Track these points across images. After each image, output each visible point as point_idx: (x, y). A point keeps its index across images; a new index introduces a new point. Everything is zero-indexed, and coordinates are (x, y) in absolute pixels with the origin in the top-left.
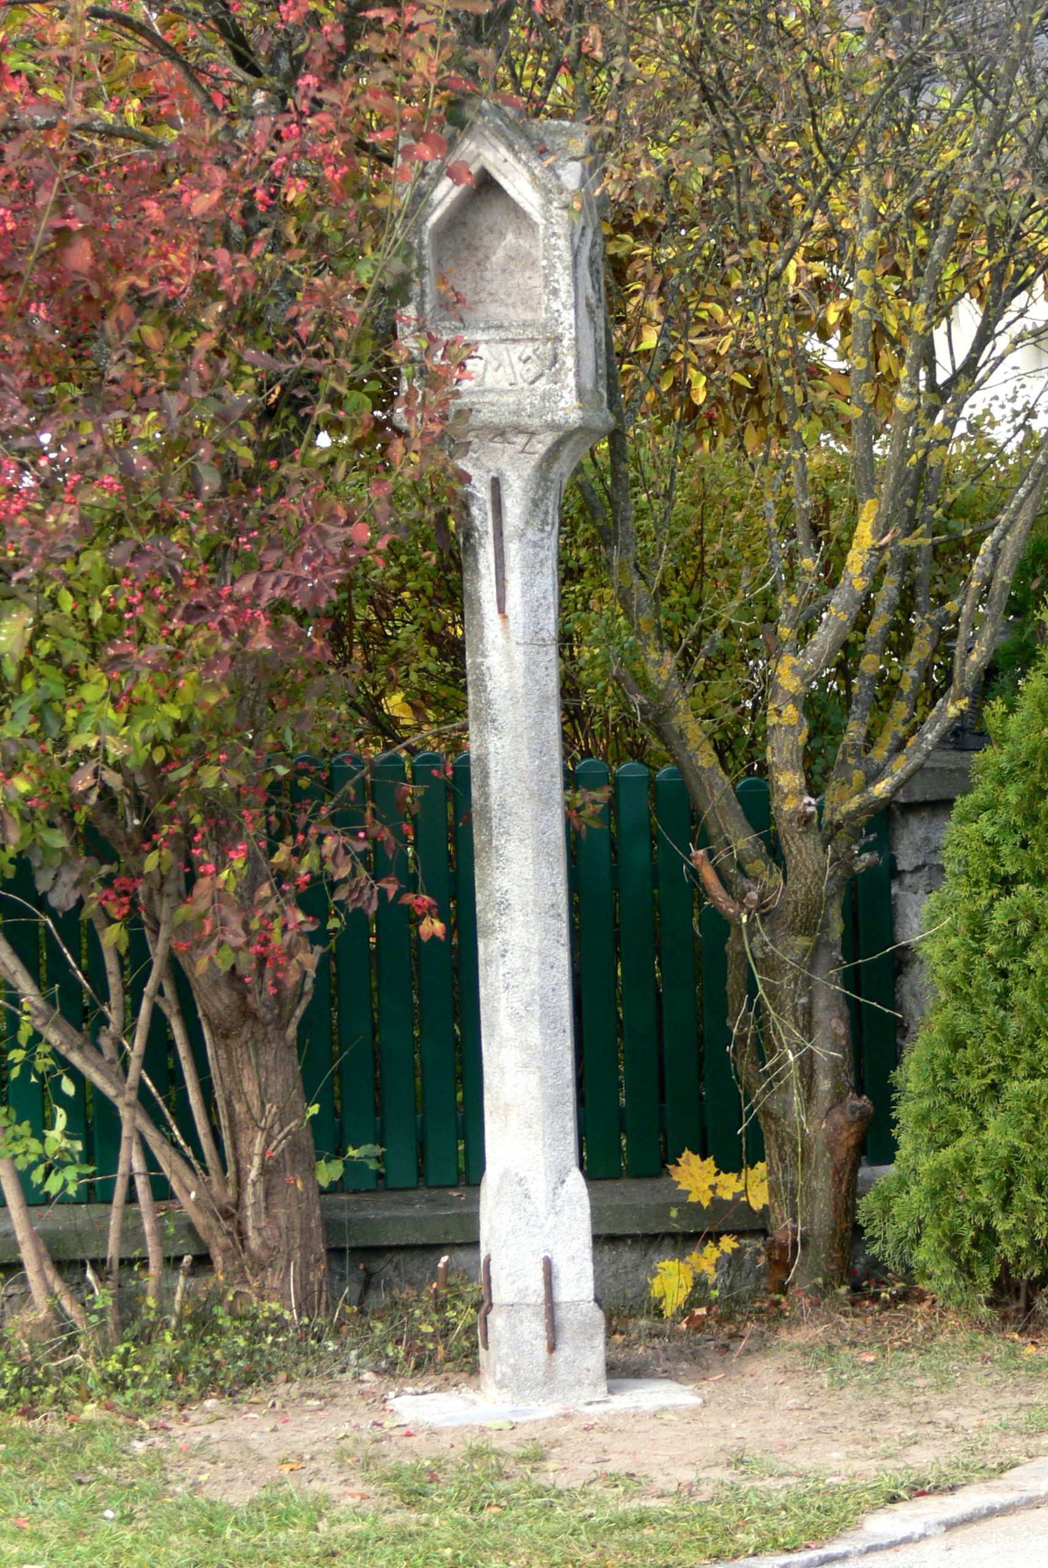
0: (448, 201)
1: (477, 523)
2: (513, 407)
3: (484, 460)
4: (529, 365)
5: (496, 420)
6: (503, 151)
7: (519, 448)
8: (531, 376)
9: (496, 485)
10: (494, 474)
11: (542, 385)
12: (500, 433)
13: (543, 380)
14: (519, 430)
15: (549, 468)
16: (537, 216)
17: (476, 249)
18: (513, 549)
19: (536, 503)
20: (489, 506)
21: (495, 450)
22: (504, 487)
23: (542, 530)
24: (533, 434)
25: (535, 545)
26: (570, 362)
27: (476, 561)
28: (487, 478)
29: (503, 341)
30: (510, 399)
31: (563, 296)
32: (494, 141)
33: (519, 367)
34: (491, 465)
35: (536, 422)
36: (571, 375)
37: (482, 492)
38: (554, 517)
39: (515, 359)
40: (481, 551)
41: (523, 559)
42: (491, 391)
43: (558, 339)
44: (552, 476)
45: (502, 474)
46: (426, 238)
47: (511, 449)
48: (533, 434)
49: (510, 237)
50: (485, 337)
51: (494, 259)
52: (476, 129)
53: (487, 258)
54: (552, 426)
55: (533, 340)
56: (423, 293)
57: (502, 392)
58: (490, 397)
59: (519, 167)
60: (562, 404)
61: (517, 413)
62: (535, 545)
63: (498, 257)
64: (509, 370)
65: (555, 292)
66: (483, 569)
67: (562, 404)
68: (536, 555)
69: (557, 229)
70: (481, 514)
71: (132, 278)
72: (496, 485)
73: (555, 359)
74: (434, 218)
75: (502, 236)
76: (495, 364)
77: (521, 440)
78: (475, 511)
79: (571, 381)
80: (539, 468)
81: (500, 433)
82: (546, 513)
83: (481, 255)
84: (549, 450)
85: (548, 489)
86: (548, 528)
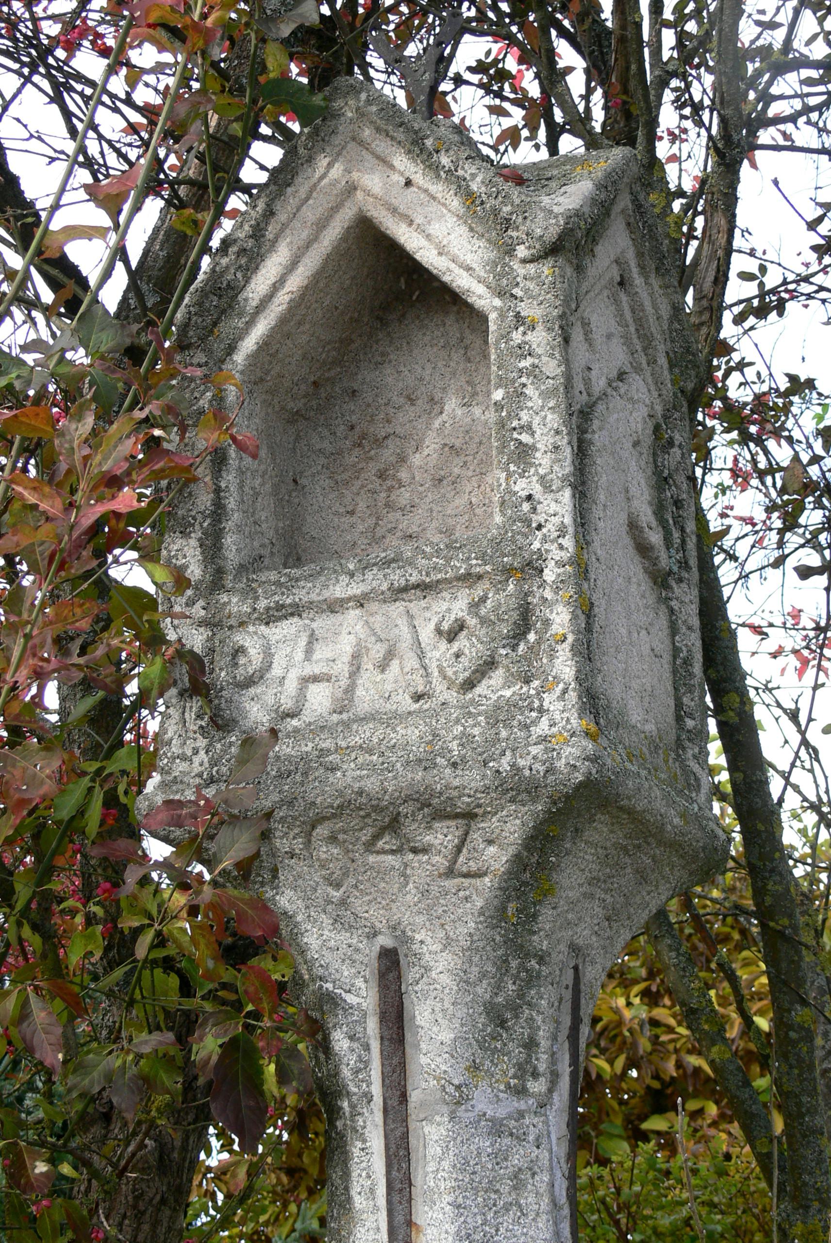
0: (282, 300)
1: (346, 1073)
2: (418, 750)
3: (358, 904)
4: (462, 642)
5: (371, 784)
6: (403, 163)
7: (440, 861)
8: (462, 671)
9: (391, 967)
10: (385, 940)
11: (495, 687)
12: (387, 821)
13: (497, 677)
14: (438, 808)
15: (529, 918)
16: (481, 297)
17: (379, 442)
18: (435, 1141)
19: (498, 1017)
20: (372, 1026)
21: (382, 873)
22: (411, 974)
23: (521, 1092)
24: (469, 816)
25: (497, 1128)
26: (561, 619)
27: (346, 1175)
28: (370, 951)
29: (399, 592)
30: (411, 733)
31: (543, 460)
32: (382, 146)
33: (439, 652)
34: (376, 916)
35: (472, 779)
36: (564, 652)
37: (361, 996)
38: (552, 1054)
39: (427, 633)
40: (356, 1150)
41: (463, 1165)
42: (370, 717)
43: (532, 568)
44: (540, 942)
45: (405, 940)
46: (232, 393)
47: (422, 868)
48: (469, 816)
49: (452, 404)
50: (357, 589)
51: (416, 460)
52: (344, 129)
53: (402, 459)
54: (517, 788)
55: (469, 579)
56: (218, 511)
57: (392, 719)
58: (363, 734)
59: (437, 188)
60: (543, 727)
61: (427, 763)
62: (497, 1128)
63: (426, 455)
64: (412, 662)
65: (523, 454)
66: (359, 1202)
67: (543, 727)
68: (500, 1157)
69: (527, 309)
70: (355, 1051)
71: (205, 871)
72: (391, 967)
73: (525, 620)
74: (249, 344)
75: (435, 404)
76: (378, 651)
77: (442, 837)
78: (340, 1042)
79: (564, 666)
80: (496, 915)
81: (387, 821)
82: (531, 1045)
83: (388, 454)
84: (519, 864)
85: (531, 980)
86: (537, 1087)
